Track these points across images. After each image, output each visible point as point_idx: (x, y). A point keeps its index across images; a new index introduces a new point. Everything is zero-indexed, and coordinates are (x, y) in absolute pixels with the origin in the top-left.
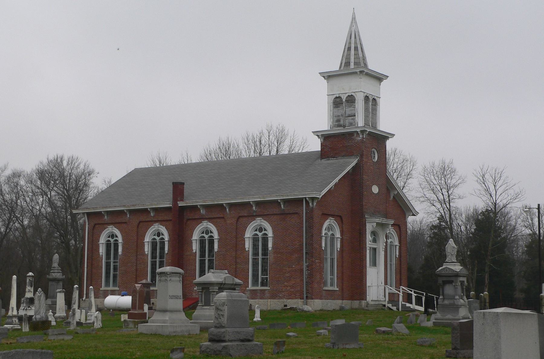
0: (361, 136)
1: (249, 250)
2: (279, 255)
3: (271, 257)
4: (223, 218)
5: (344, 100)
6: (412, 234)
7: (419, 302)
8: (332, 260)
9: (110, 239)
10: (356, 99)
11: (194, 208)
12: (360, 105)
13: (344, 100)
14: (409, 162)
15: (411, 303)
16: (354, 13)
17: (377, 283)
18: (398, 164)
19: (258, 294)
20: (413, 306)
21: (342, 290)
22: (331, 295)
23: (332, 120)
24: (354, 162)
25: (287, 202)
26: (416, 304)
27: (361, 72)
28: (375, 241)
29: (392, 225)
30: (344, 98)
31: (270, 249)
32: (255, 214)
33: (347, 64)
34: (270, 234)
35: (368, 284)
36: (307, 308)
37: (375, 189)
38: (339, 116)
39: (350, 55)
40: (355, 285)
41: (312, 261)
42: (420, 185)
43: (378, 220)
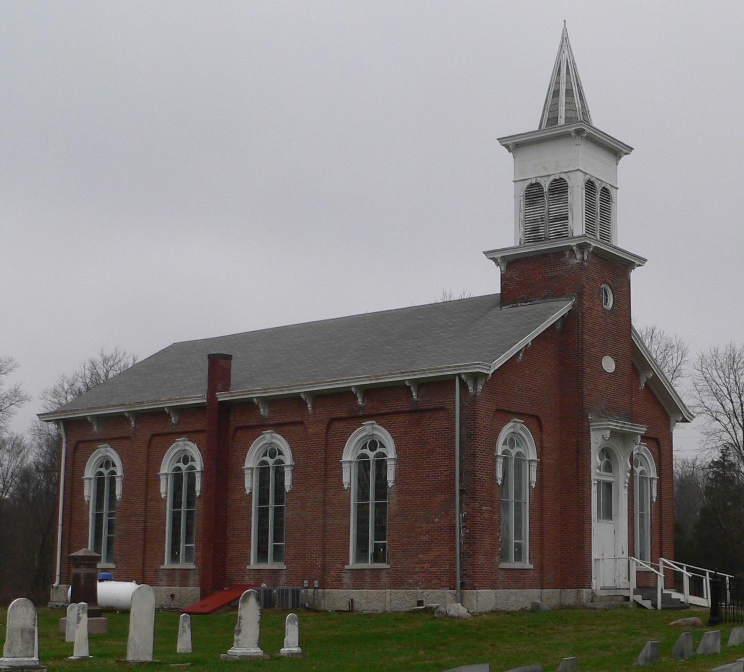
0: (579, 256)
1: (349, 489)
2: (407, 498)
3: (392, 502)
4: (301, 423)
5: (546, 189)
6: (681, 480)
7: (696, 590)
8: (518, 506)
9: (181, 465)
10: (570, 184)
11: (247, 405)
12: (577, 198)
13: (546, 189)
14: (675, 350)
15: (681, 590)
16: (565, 30)
17: (613, 556)
18: (658, 353)
19: (368, 579)
20: (686, 597)
21: (540, 567)
22: (516, 579)
23: (522, 229)
24: (564, 308)
25: (424, 385)
26: (691, 594)
27: (579, 132)
28: (608, 468)
29: (644, 438)
30: (546, 184)
31: (390, 485)
32: (361, 413)
33: (553, 120)
34: (391, 453)
35: (594, 556)
36: (457, 609)
37: (609, 364)
38: (535, 221)
39: (557, 104)
40: (566, 556)
41: (474, 509)
42: (695, 385)
43: (613, 425)
